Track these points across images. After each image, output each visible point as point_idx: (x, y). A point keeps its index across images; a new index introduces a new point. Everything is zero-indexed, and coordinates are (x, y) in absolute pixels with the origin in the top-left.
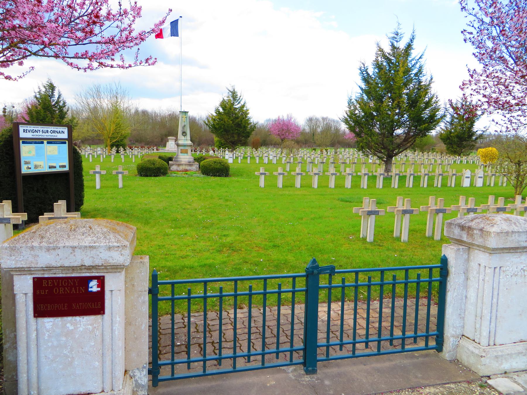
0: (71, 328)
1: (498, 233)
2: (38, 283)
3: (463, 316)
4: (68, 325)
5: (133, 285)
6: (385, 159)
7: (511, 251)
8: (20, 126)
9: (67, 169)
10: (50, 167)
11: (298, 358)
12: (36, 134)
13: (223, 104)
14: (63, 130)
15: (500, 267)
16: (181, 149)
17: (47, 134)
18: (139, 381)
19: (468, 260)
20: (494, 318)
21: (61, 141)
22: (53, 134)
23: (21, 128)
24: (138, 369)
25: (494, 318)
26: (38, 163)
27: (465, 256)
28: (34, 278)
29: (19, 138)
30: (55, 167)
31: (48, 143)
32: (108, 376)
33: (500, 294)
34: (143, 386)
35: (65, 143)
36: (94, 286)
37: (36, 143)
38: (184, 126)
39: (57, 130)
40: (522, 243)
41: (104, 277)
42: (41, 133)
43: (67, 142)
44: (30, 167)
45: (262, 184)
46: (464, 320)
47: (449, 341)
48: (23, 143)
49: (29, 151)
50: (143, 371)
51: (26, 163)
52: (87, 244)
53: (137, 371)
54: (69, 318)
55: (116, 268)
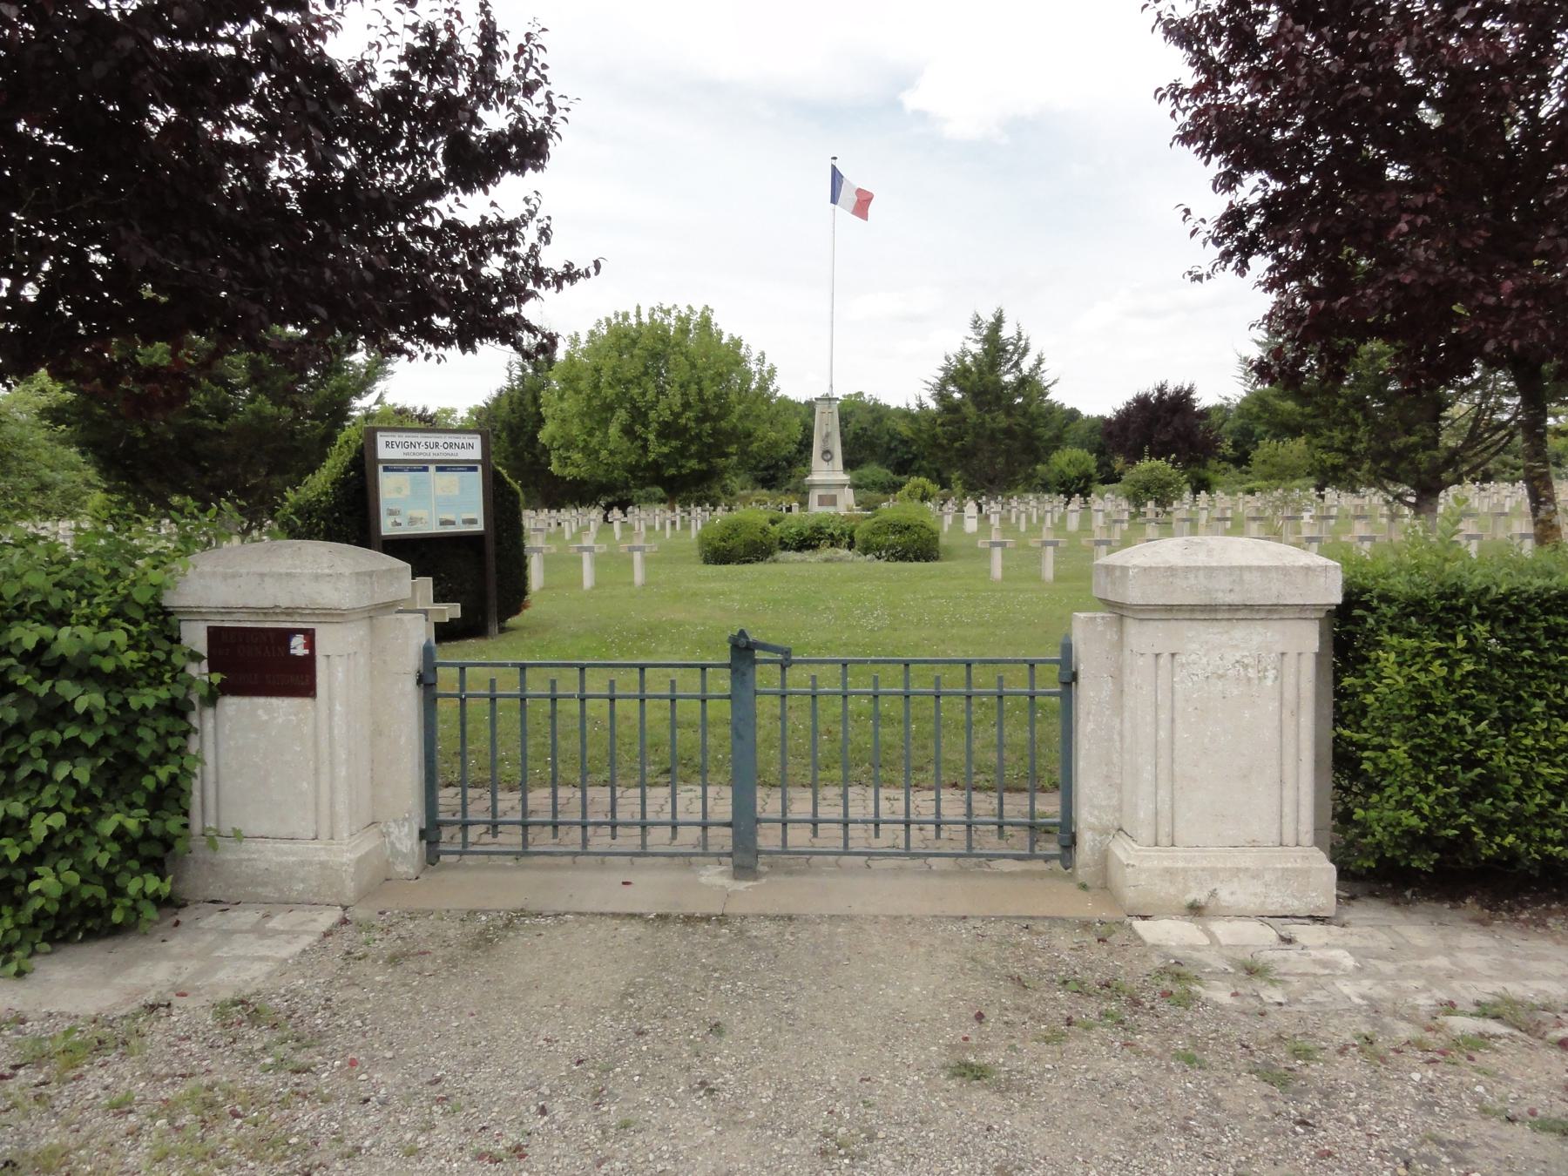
0: (265, 718)
1: (1145, 569)
2: (215, 634)
3: (1118, 781)
4: (260, 712)
5: (385, 662)
6: (1412, 500)
7: (1198, 615)
8: (379, 434)
9: (479, 527)
10: (444, 523)
11: (722, 838)
12: (412, 450)
13: (957, 375)
14: (471, 441)
15: (1173, 655)
16: (820, 496)
17: (434, 450)
18: (398, 845)
19: (1120, 644)
20: (1163, 776)
21: (469, 466)
22: (449, 451)
23: (382, 439)
24: (395, 821)
25: (1163, 776)
26: (416, 513)
27: (1111, 635)
28: (209, 628)
29: (376, 461)
30: (453, 523)
31: (439, 469)
32: (325, 810)
33: (1178, 721)
34: (405, 855)
35: (475, 469)
36: (298, 647)
37: (411, 470)
38: (828, 435)
39: (457, 441)
40: (1220, 595)
41: (313, 630)
42: (423, 450)
43: (480, 467)
44: (398, 521)
45: (997, 571)
46: (1120, 791)
47: (1087, 841)
48: (386, 469)
49: (399, 490)
50: (403, 825)
51: (392, 513)
52: (283, 570)
53: (393, 825)
54: (261, 701)
55: (333, 615)
